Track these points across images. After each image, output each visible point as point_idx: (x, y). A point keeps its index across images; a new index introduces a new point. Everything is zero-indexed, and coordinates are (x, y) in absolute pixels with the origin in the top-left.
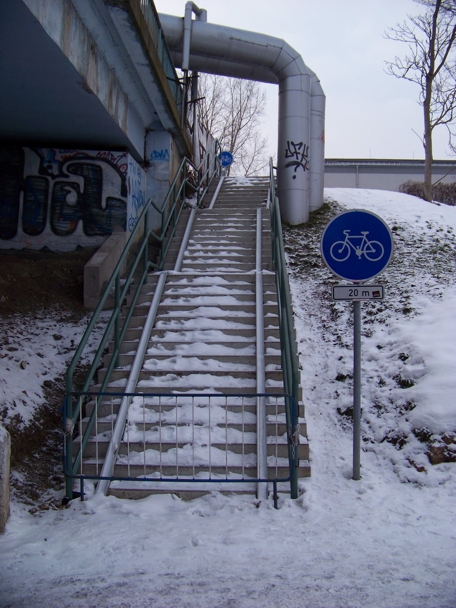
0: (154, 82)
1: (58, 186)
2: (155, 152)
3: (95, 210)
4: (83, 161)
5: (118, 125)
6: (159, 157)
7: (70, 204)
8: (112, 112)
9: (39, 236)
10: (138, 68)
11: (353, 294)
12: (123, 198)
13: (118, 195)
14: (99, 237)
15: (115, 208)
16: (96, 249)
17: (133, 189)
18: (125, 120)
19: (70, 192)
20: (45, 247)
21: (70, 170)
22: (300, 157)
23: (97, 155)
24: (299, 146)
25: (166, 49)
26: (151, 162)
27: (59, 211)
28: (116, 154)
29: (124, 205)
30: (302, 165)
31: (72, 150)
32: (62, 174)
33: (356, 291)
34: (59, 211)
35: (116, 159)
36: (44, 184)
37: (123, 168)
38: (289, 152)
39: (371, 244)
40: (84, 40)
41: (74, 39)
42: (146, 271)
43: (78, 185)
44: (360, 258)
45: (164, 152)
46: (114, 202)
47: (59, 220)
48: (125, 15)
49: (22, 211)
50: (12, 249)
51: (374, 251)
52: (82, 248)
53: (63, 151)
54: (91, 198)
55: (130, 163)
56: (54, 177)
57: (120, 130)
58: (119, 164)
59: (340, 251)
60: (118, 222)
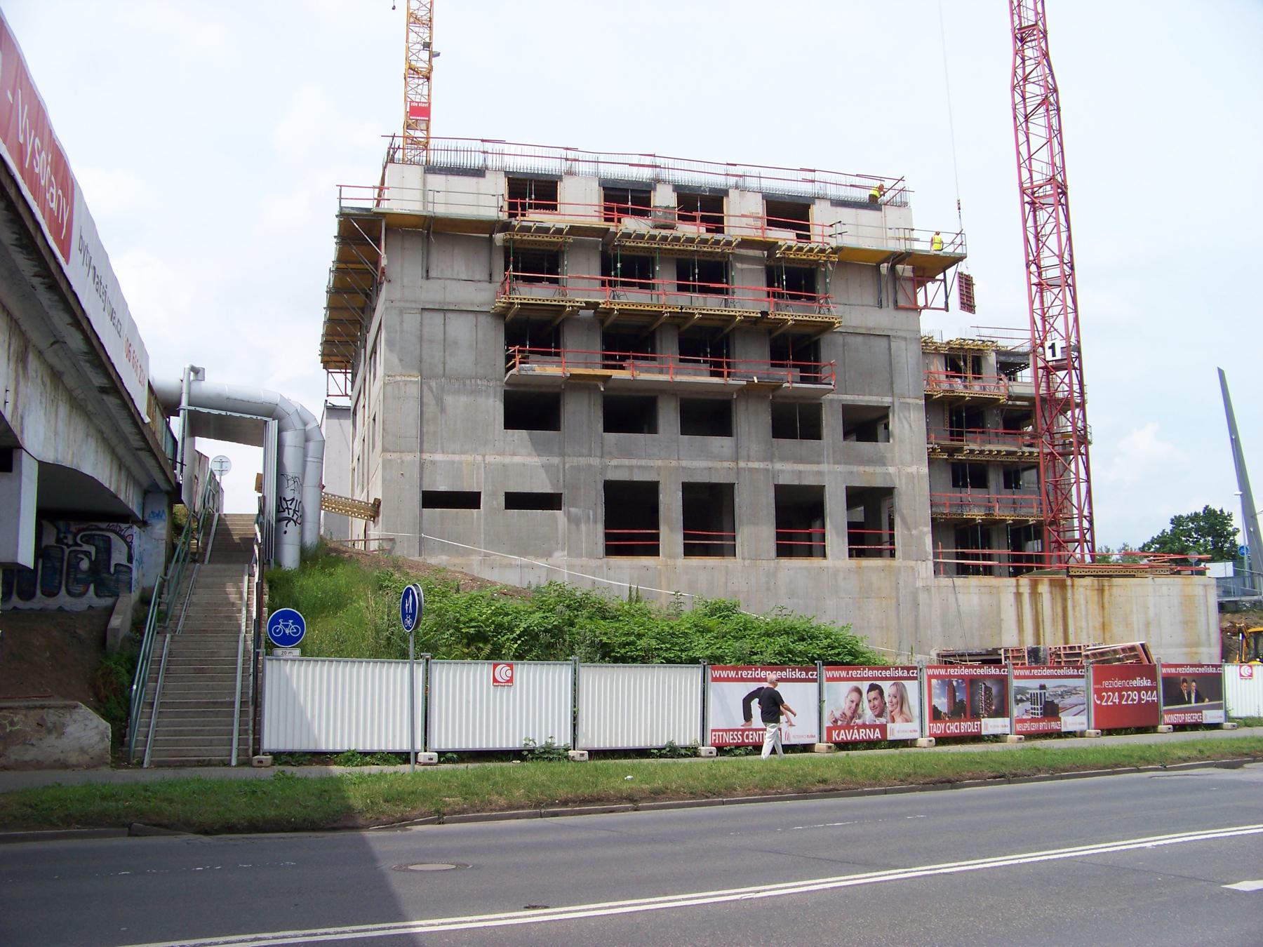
13: (125, 563)
28: (123, 526)
32: (76, 544)
56: (69, 546)
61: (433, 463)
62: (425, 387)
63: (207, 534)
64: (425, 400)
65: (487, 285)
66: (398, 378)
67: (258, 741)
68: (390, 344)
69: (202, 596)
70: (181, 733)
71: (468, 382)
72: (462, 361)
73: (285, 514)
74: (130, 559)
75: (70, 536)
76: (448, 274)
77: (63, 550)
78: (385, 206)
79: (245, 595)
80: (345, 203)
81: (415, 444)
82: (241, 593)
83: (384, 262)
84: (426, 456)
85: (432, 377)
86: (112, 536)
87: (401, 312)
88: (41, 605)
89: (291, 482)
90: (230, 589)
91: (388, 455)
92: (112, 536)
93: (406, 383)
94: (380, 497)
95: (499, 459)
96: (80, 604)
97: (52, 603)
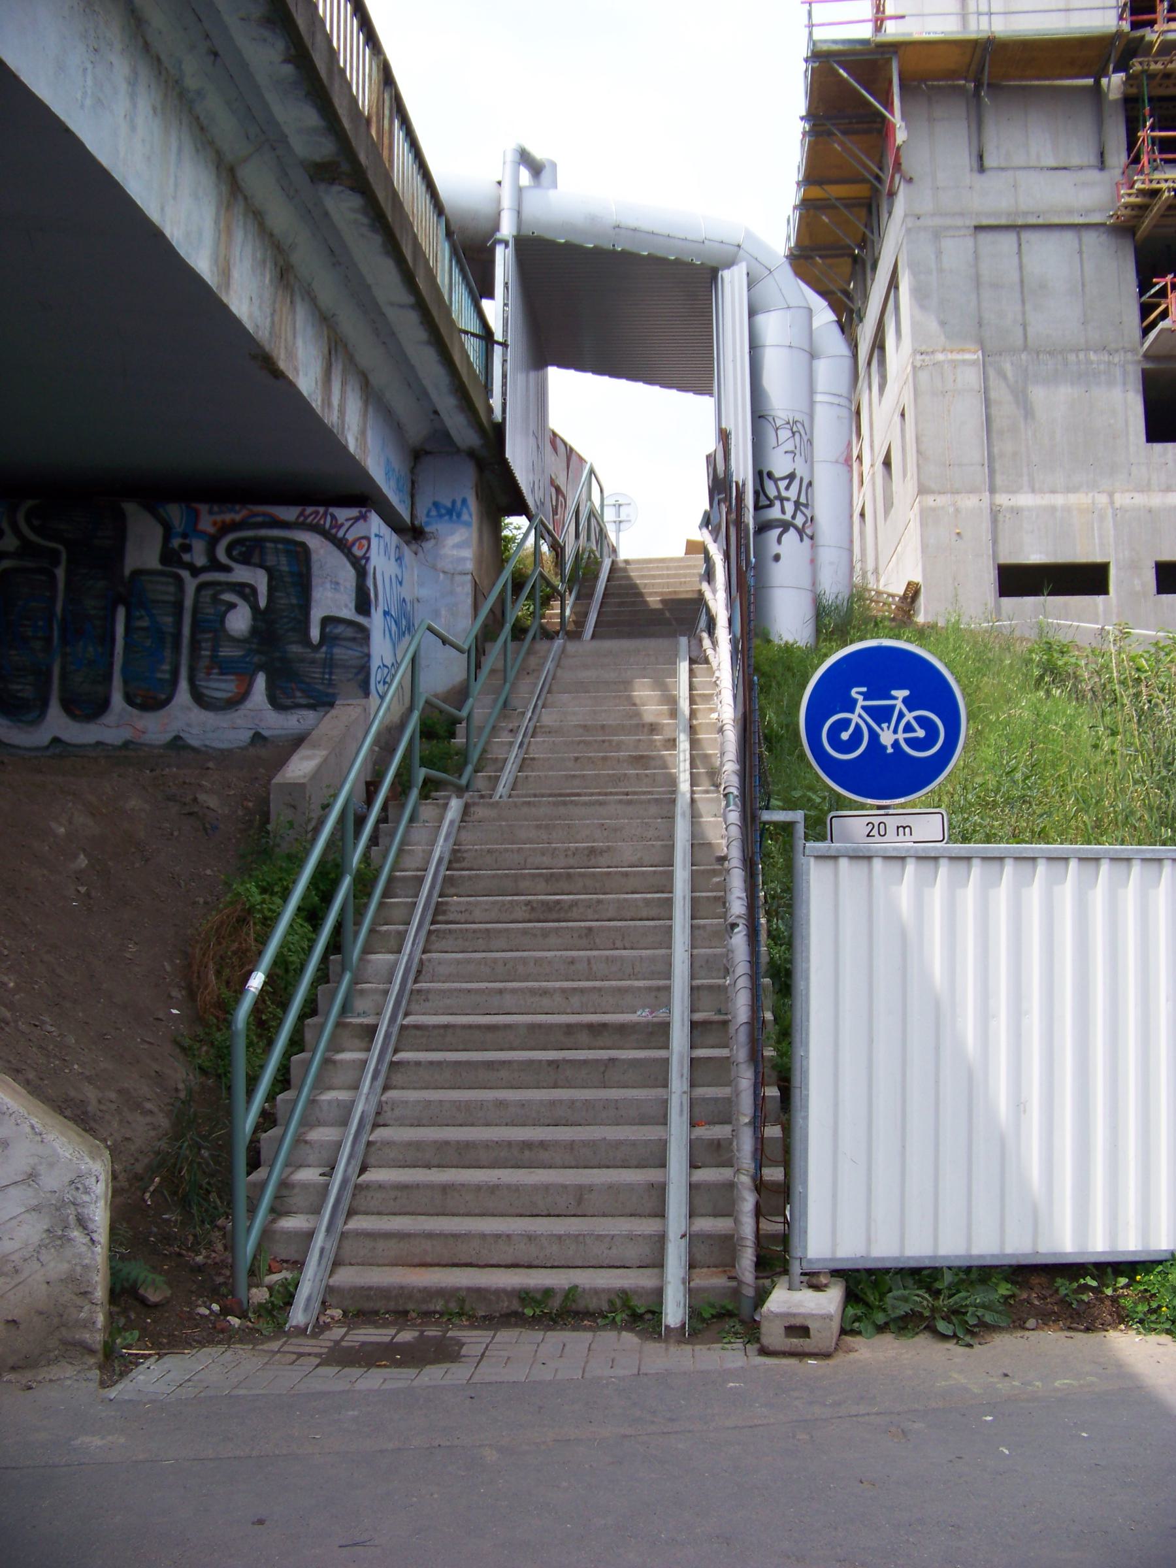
0: (429, 343)
1: (207, 593)
2: (436, 505)
3: (295, 649)
4: (263, 532)
5: (345, 448)
6: (447, 518)
7: (232, 633)
8: (331, 418)
9: (163, 712)
10: (391, 313)
11: (875, 832)
12: (361, 619)
13: (347, 612)
14: (305, 712)
15: (342, 643)
16: (298, 741)
17: (384, 595)
18: (363, 432)
19: (233, 606)
20: (178, 738)
21: (235, 553)
22: (789, 507)
23: (298, 517)
24: (787, 481)
25: (459, 262)
26: (427, 529)
27: (208, 653)
28: (343, 514)
29: (363, 634)
30: (796, 528)
31: (237, 507)
32: (215, 565)
33: (882, 826)
34: (208, 653)
35: (342, 525)
36: (172, 589)
37: (360, 547)
38: (762, 497)
39: (916, 718)
40: (264, 262)
41: (241, 260)
42: (415, 793)
43: (254, 590)
44: (890, 750)
45: (459, 504)
46: (340, 629)
47: (209, 674)
48: (356, 201)
49: (121, 652)
50: (99, 744)
51: (921, 733)
52: (264, 739)
53: (216, 508)
54: (285, 620)
55: (376, 535)
56: (195, 571)
57: (352, 457)
58: (350, 537)
59: (845, 736)
60: (350, 676)
61: (1016, 511)
62: (992, 373)
63: (585, 596)
64: (993, 395)
65: (1095, 175)
66: (940, 357)
67: (779, 1196)
68: (920, 295)
69: (570, 711)
70: (464, 1155)
71: (1072, 357)
72: (1058, 318)
73: (775, 513)
74: (363, 604)
75: (199, 546)
76: (1019, 160)
77: (179, 581)
78: (893, 31)
79: (684, 705)
80: (820, 34)
81: (980, 476)
82: (673, 701)
83: (901, 136)
84: (1002, 499)
85: (1005, 354)
86: (313, 541)
87: (937, 234)
88: (125, 734)
89: (784, 434)
90: (644, 693)
91: (929, 500)
92: (313, 541)
93: (954, 364)
94: (917, 578)
95: (1140, 499)
96: (223, 731)
97: (154, 728)
